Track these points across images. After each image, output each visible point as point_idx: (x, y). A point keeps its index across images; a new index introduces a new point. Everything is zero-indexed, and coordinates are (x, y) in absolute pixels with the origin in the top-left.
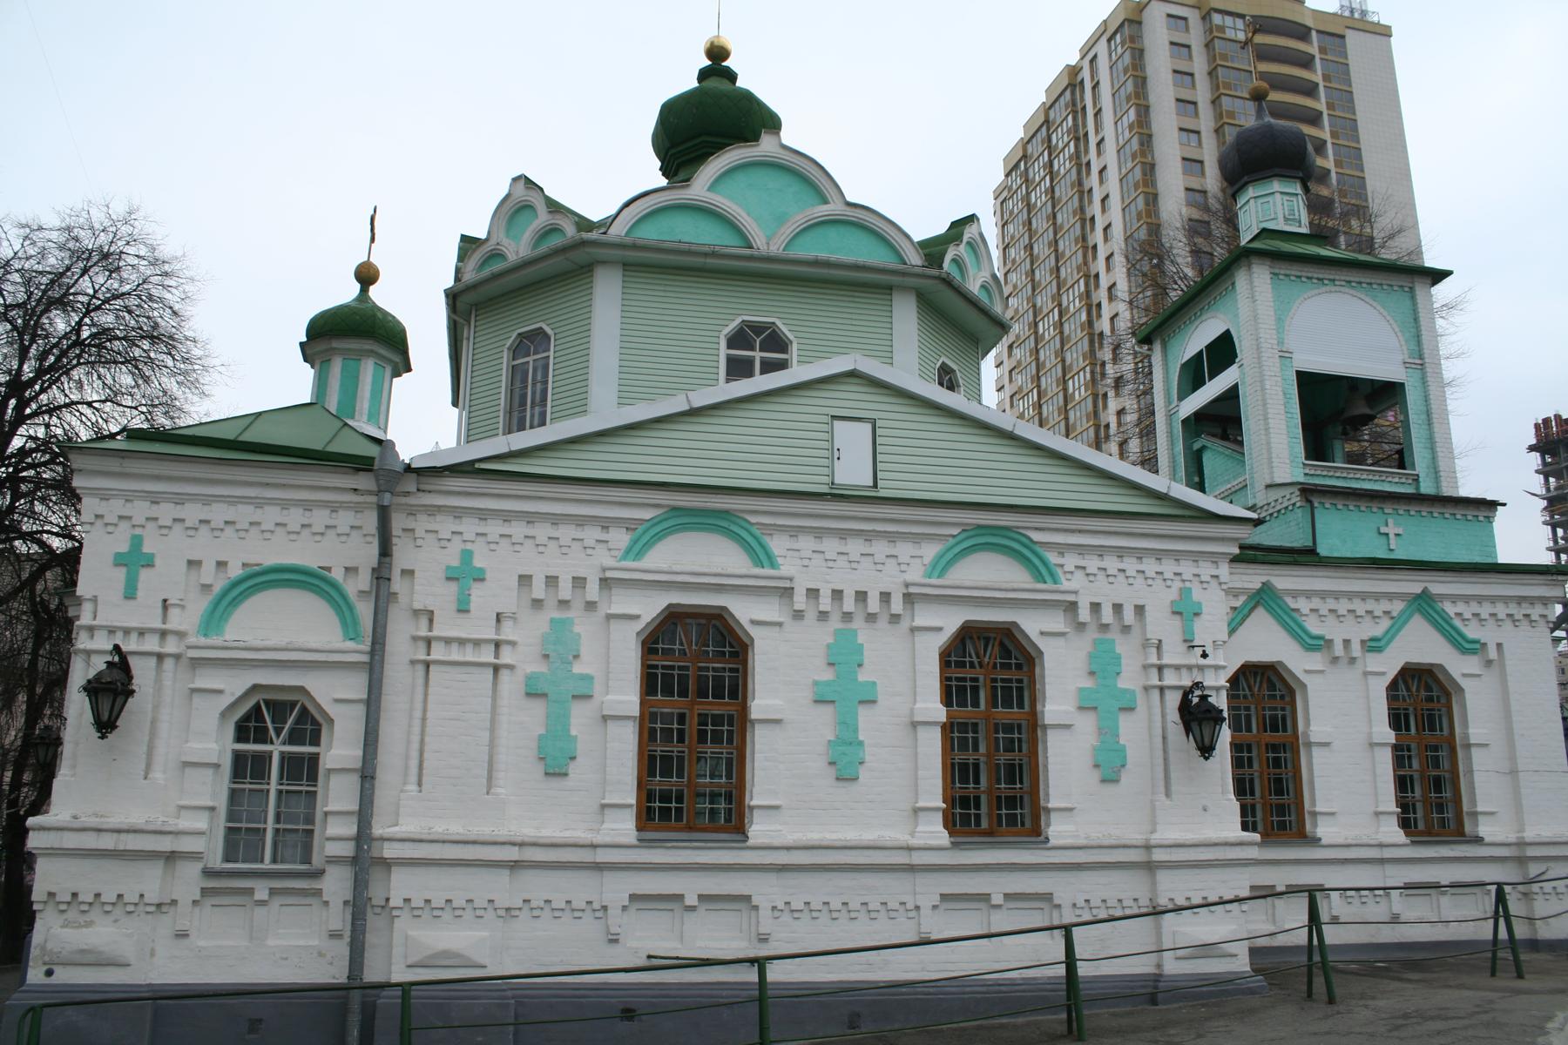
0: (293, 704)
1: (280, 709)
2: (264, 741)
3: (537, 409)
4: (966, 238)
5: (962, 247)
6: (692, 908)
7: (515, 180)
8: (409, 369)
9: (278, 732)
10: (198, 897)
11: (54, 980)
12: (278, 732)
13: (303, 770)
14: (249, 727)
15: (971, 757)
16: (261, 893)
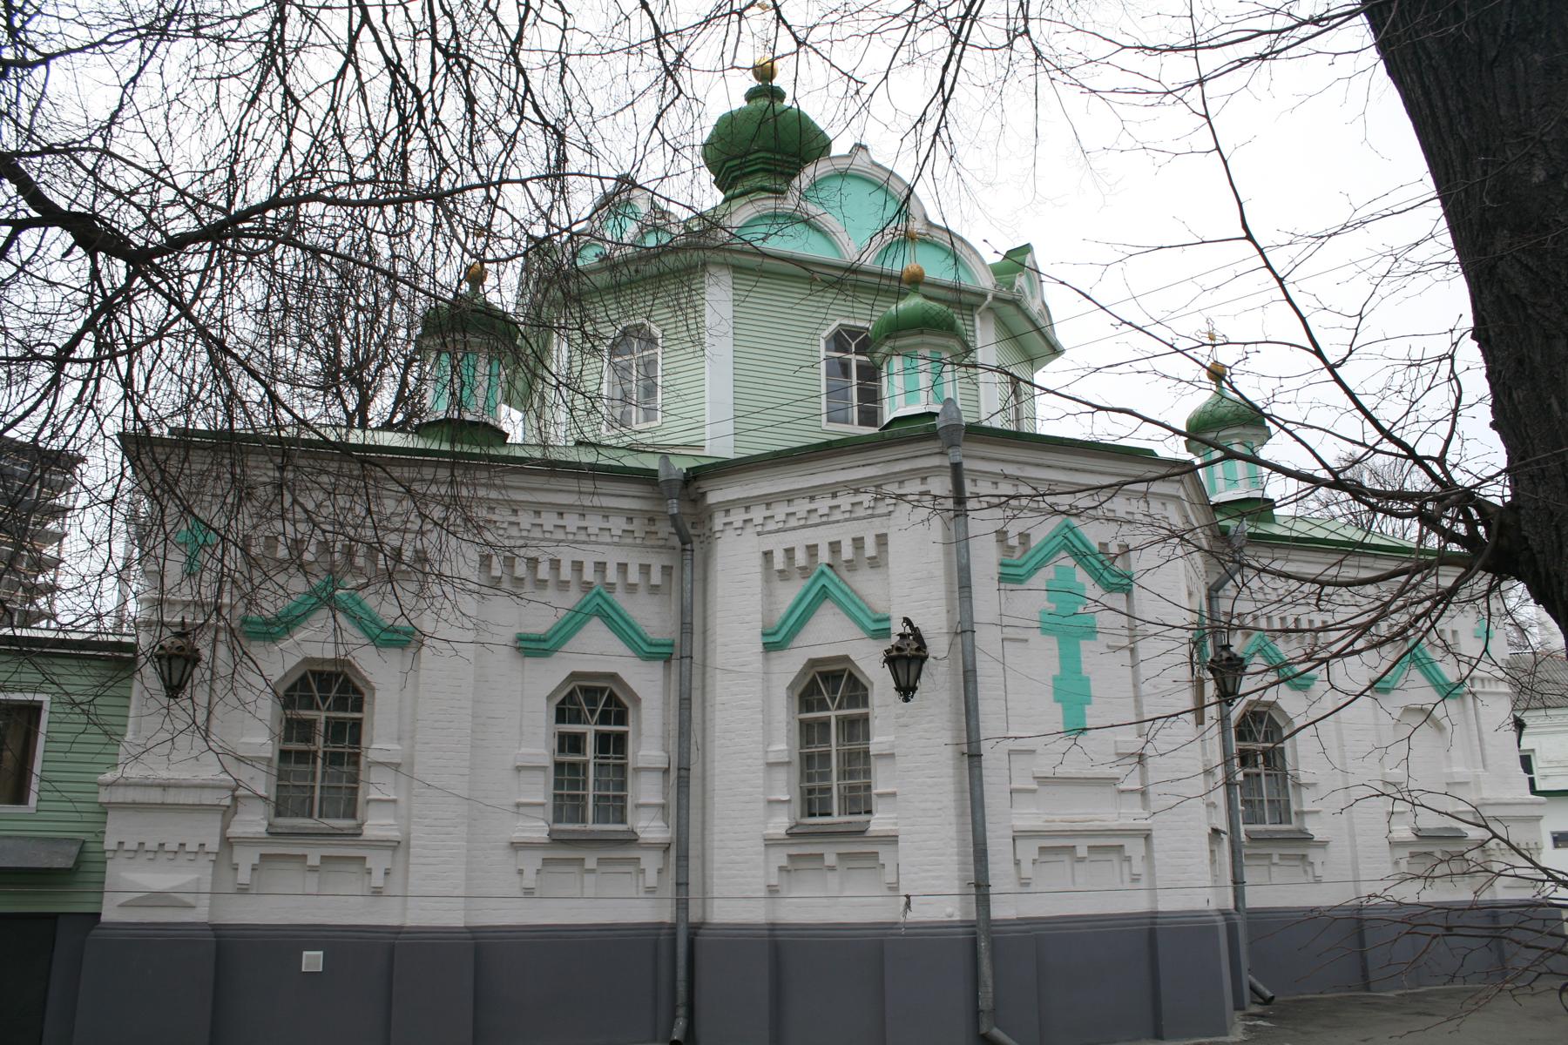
0: (602, 690)
1: (591, 694)
2: (310, 707)
6: (1082, 860)
11: (912, 916)
13: (613, 745)
14: (565, 710)
15: (1243, 745)
16: (831, 859)
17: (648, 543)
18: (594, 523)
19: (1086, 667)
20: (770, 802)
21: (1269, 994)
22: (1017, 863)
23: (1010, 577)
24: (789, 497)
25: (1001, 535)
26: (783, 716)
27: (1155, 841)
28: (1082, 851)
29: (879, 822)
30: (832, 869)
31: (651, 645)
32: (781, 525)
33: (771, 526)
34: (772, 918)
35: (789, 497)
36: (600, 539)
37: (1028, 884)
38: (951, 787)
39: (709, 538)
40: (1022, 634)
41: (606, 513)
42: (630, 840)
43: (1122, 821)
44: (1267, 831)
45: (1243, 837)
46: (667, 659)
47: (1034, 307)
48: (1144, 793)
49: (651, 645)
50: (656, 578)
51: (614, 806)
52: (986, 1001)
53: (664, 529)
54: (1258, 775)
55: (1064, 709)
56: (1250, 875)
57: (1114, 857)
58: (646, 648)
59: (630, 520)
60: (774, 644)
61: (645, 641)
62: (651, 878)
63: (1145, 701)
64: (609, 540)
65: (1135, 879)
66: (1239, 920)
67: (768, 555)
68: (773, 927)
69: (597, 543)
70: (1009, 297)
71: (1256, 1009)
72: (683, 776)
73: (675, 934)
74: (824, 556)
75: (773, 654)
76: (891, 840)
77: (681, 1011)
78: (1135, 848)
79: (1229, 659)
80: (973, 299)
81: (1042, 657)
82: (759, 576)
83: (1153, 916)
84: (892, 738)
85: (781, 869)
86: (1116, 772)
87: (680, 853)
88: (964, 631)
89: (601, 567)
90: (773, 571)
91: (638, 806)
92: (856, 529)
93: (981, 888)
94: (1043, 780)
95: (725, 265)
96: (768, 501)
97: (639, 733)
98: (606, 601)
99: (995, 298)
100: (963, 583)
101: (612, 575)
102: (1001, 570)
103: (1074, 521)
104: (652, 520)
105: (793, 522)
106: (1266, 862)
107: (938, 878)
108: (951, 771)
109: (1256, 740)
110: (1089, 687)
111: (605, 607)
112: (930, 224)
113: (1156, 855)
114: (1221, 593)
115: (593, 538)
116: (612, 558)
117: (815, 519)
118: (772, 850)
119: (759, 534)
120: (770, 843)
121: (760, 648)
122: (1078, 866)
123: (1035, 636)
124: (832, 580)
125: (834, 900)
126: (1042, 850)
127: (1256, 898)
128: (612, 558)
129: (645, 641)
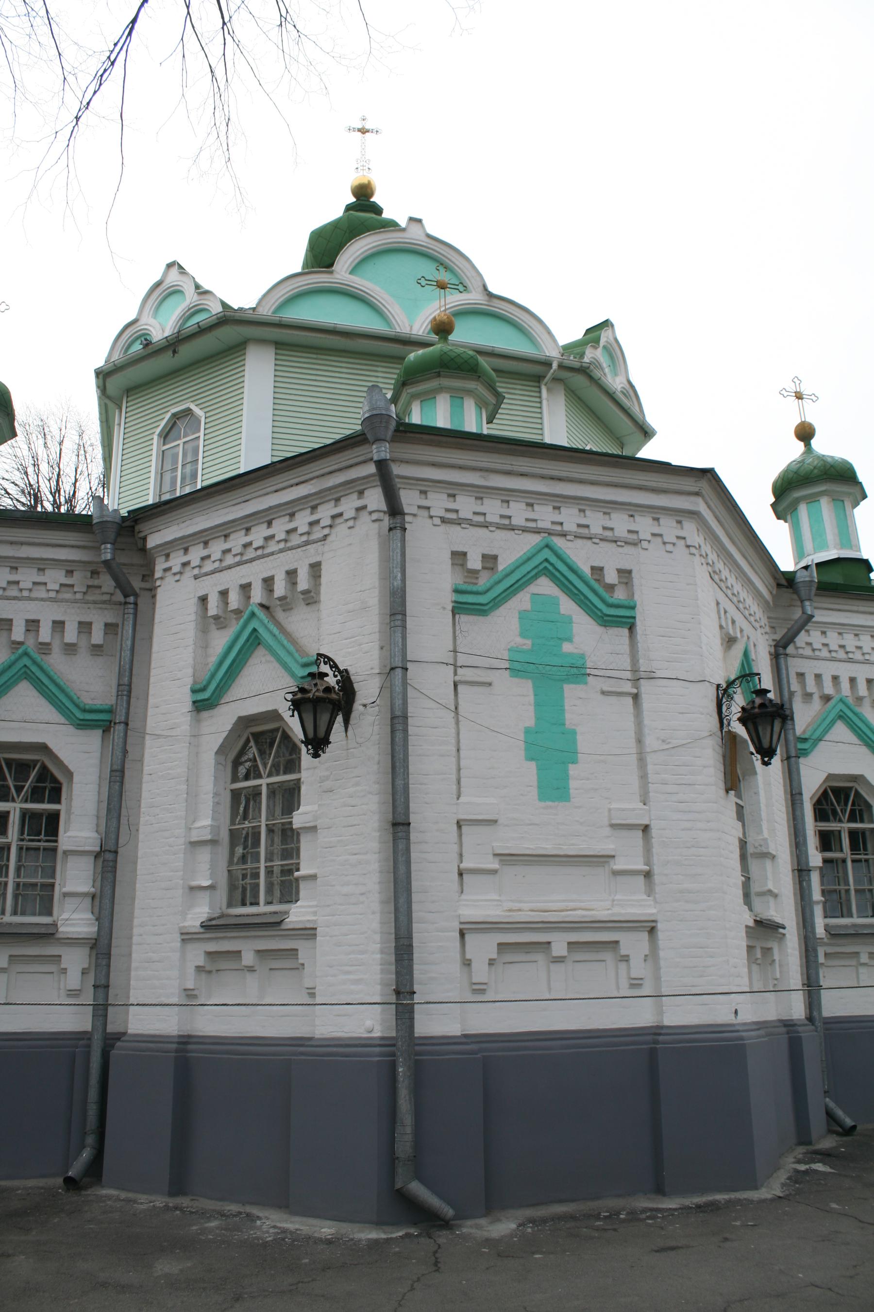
0: (33, 764)
3: (188, 468)
4: (603, 342)
5: (600, 350)
6: (560, 960)
7: (170, 266)
8: (864, 496)
9: (19, 789)
10: (494, 956)
12: (19, 789)
13: (51, 824)
16: (248, 958)
17: (89, 598)
18: (27, 577)
19: (570, 718)
20: (192, 889)
21: (849, 1122)
22: (467, 963)
23: (465, 606)
24: (224, 531)
25: (459, 557)
26: (210, 786)
27: (661, 935)
28: (559, 948)
29: (298, 914)
30: (251, 969)
31: (85, 711)
32: (217, 565)
33: (208, 567)
34: (187, 1030)
35: (224, 531)
36: (34, 595)
37: (482, 991)
38: (375, 866)
39: (152, 591)
40: (483, 676)
41: (41, 564)
42: (48, 935)
43: (616, 910)
44: (854, 926)
45: (820, 931)
46: (107, 728)
47: (616, 383)
48: (648, 875)
49: (85, 711)
50: (97, 636)
51: (42, 896)
52: (404, 1146)
53: (107, 583)
54: (844, 861)
55: (538, 769)
56: (827, 978)
57: (608, 956)
58: (80, 715)
59: (69, 573)
60: (204, 703)
61: (77, 706)
62: (73, 979)
63: (650, 759)
64: (44, 595)
65: (636, 983)
66: (806, 1032)
67: (203, 600)
68: (185, 1041)
69: (29, 599)
70: (577, 365)
71: (828, 1143)
72: (109, 858)
73: (89, 1046)
74: (257, 595)
75: (205, 714)
76: (309, 933)
77: (90, 1140)
78: (634, 945)
79: (762, 705)
80: (538, 369)
81: (511, 705)
82: (192, 625)
83: (657, 1031)
84: (316, 807)
85: (199, 969)
86: (605, 846)
87: (102, 949)
88: (396, 668)
89: (33, 625)
90: (208, 622)
91: (66, 895)
92: (288, 561)
93: (403, 996)
94: (508, 859)
95: (262, 341)
96: (204, 538)
97: (69, 812)
98: (34, 662)
99: (561, 366)
100: (396, 610)
101: (45, 634)
102: (455, 597)
103: (558, 542)
104: (95, 573)
105: (229, 560)
106: (854, 962)
107: (357, 982)
108: (375, 845)
109: (840, 821)
110: (575, 742)
111: (34, 669)
112: (491, 295)
113: (662, 954)
114: (790, 649)
115: (25, 593)
116: (47, 615)
117: (250, 554)
118: (190, 946)
119: (196, 577)
120: (187, 937)
121: (188, 706)
122: (553, 967)
123: (503, 681)
124: (261, 622)
125: (248, 1011)
126: (502, 947)
127: (837, 1004)
128: (47, 615)
129: (77, 706)
